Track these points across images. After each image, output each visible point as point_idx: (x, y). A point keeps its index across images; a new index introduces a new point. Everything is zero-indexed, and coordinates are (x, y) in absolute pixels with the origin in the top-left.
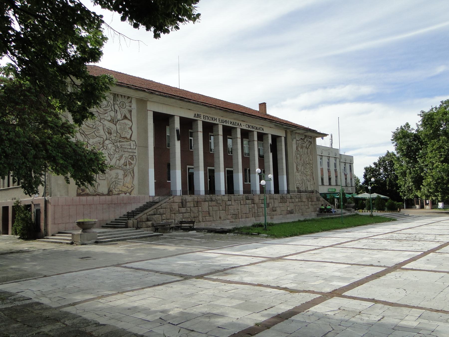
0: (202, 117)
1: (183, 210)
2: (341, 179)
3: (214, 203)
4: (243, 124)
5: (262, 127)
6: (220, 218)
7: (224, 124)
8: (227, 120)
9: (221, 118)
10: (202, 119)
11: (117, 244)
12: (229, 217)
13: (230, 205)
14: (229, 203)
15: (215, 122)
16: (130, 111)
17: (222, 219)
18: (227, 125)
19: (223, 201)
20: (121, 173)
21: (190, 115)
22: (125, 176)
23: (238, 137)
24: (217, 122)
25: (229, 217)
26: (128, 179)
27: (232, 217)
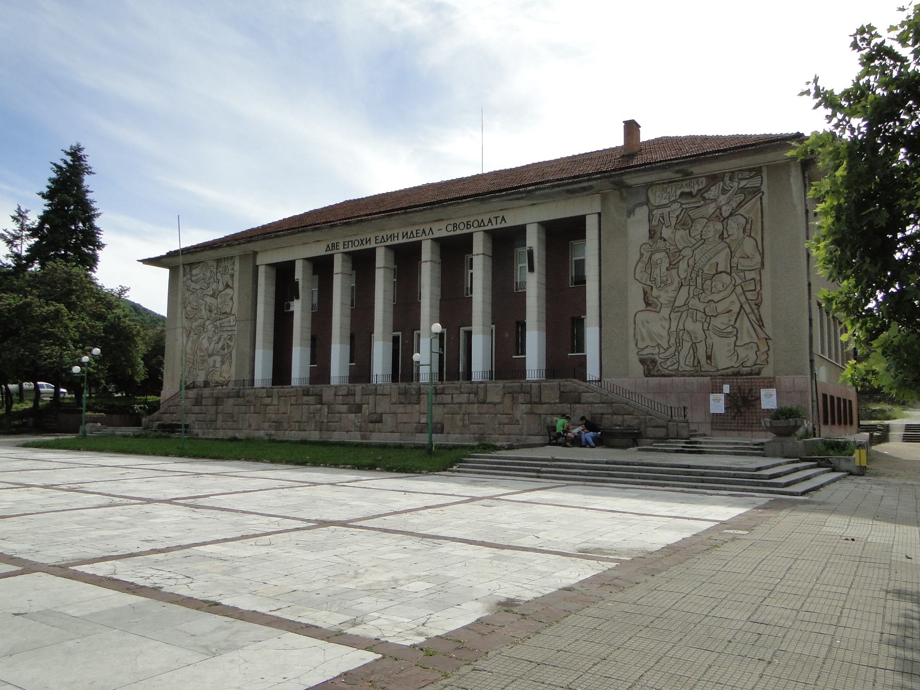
0: (341, 247)
1: (196, 409)
2: (56, 496)
3: (241, 401)
4: (435, 226)
5: (501, 214)
6: (250, 426)
7: (389, 243)
8: (395, 232)
9: (380, 234)
10: (341, 249)
11: (169, 437)
12: (266, 425)
13: (268, 405)
14: (268, 401)
15: (368, 246)
16: (232, 276)
17: (253, 427)
18: (396, 242)
19: (256, 397)
20: (218, 359)
21: (319, 250)
22: (223, 362)
23: (429, 264)
24: (373, 245)
25: (266, 425)
26: (225, 367)
27: (270, 426)
